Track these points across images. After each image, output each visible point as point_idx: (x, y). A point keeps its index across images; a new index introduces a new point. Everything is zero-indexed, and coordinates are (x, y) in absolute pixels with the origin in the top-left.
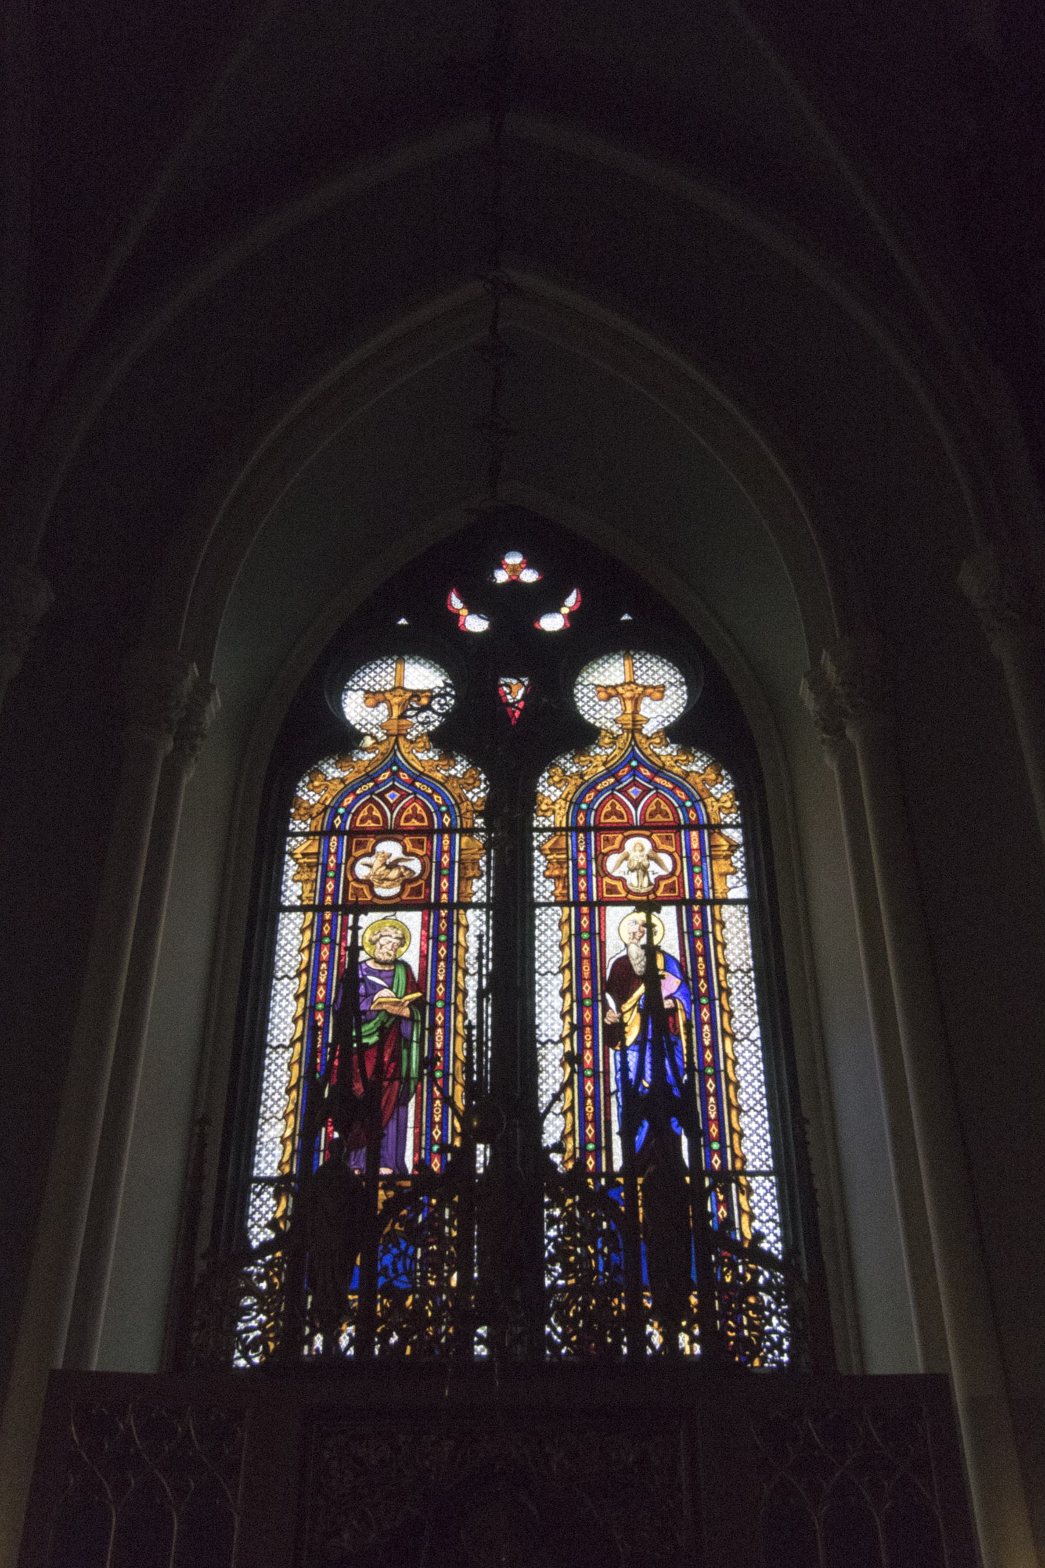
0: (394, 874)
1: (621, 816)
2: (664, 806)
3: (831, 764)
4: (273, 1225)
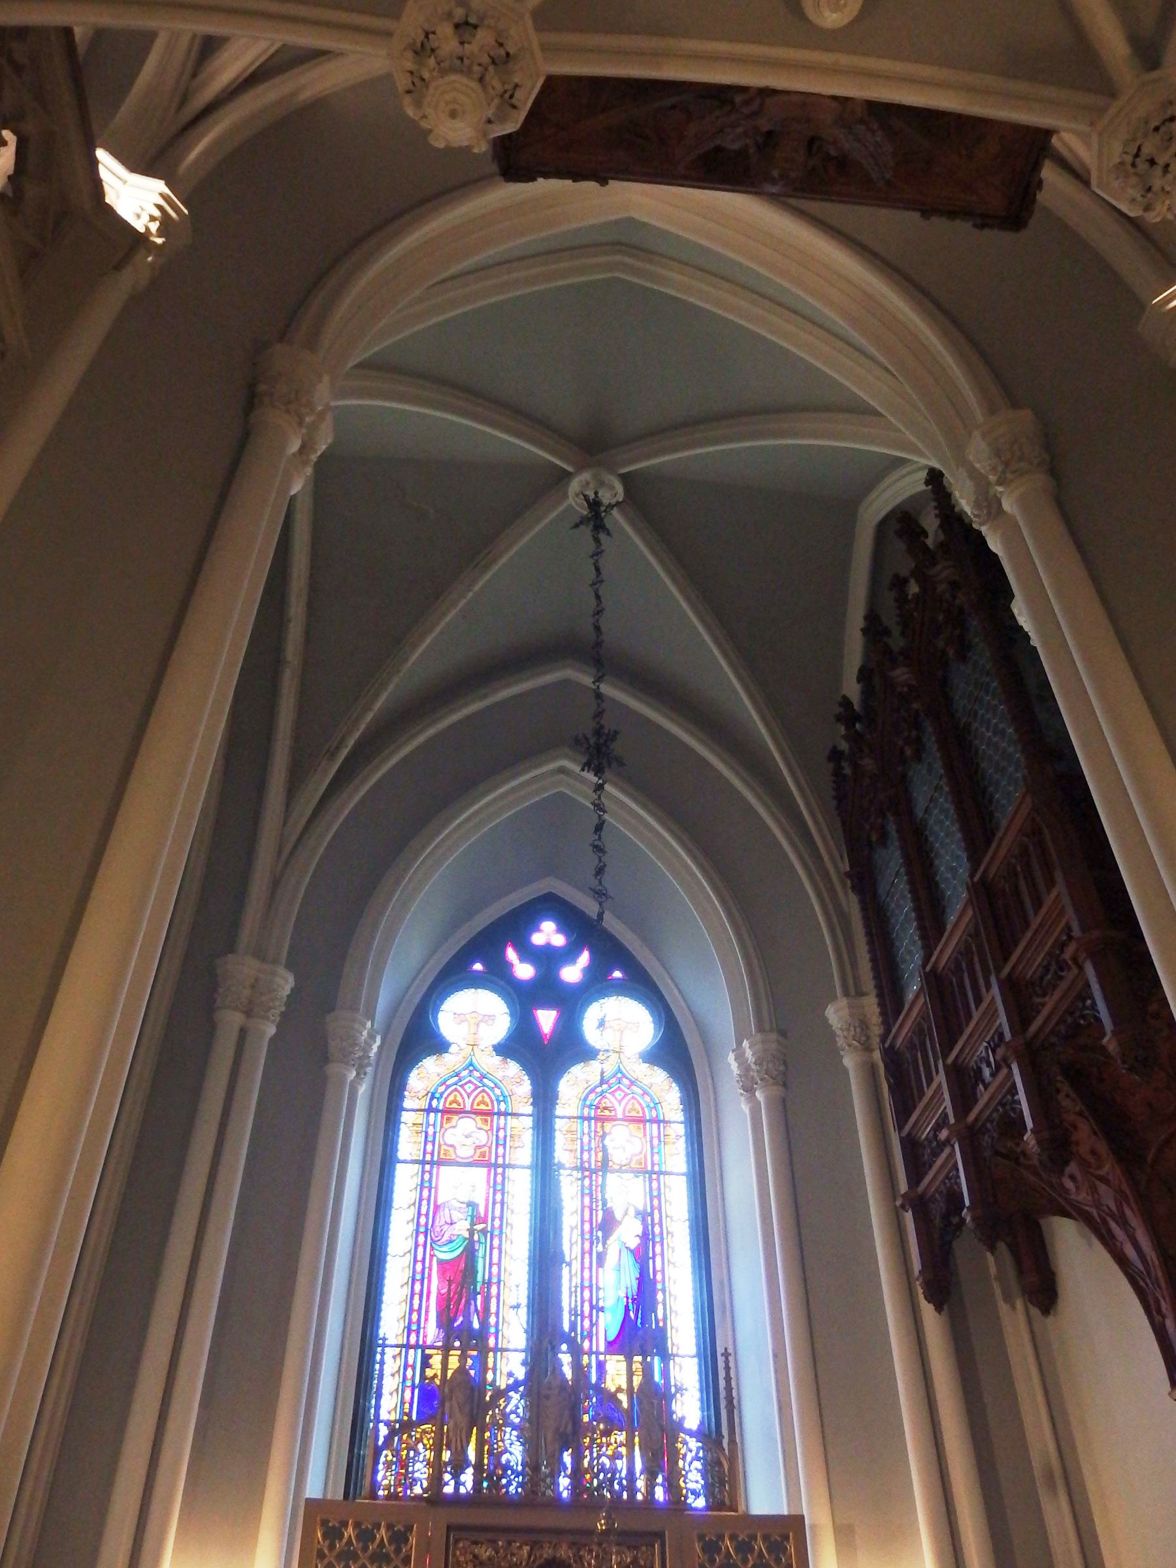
0: (469, 1141)
3: (745, 1108)
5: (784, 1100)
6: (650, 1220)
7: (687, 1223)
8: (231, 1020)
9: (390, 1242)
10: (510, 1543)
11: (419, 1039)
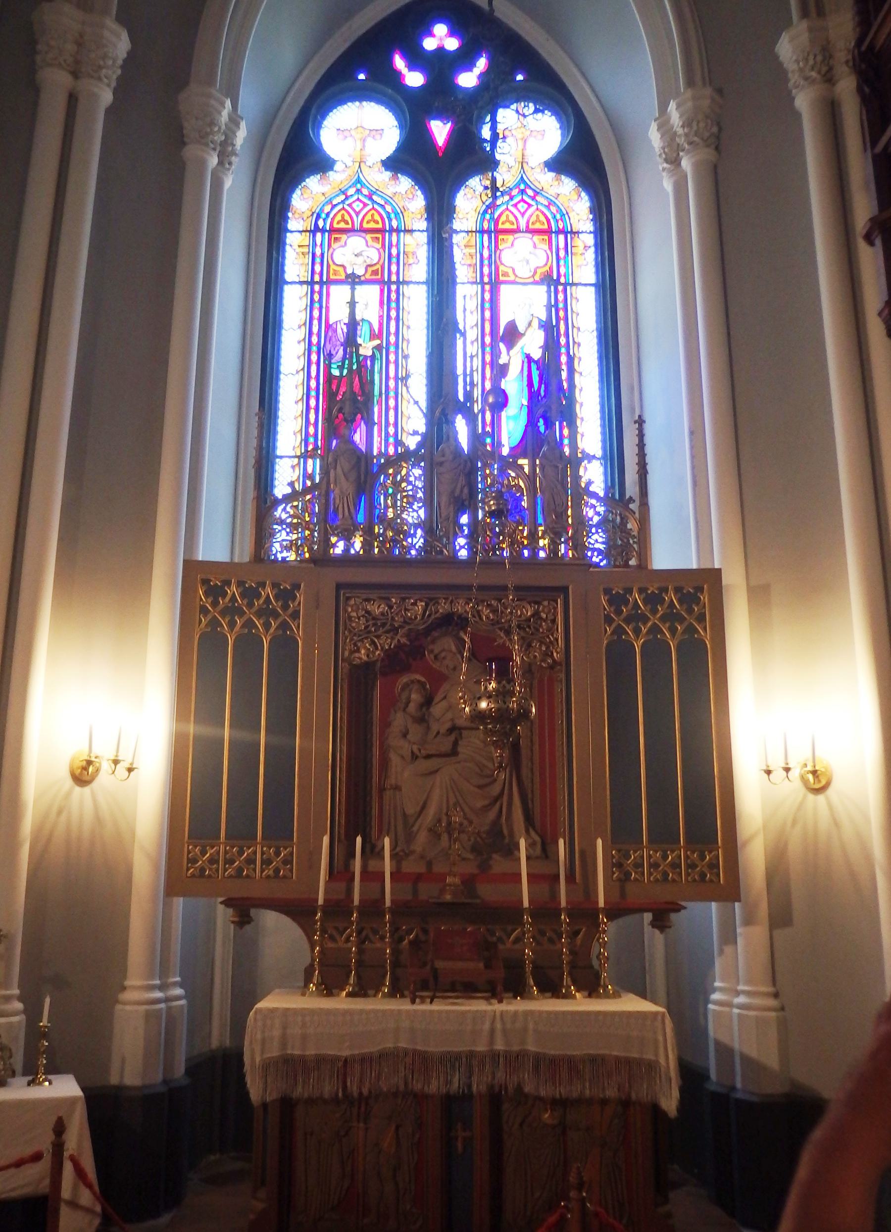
0: (360, 260)
1: (347, 223)
2: (347, 217)
3: (668, 185)
4: (291, 484)
5: (715, 167)
6: (554, 333)
7: (595, 333)
8: (55, 81)
9: (282, 361)
10: (403, 599)
11: (298, 157)
